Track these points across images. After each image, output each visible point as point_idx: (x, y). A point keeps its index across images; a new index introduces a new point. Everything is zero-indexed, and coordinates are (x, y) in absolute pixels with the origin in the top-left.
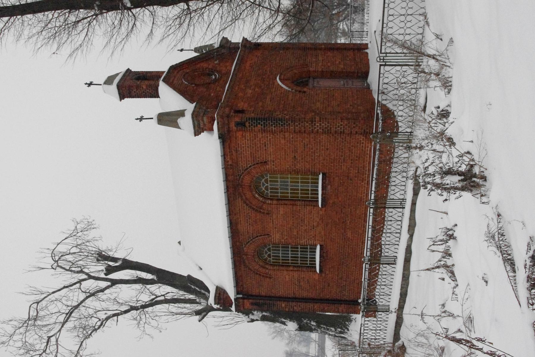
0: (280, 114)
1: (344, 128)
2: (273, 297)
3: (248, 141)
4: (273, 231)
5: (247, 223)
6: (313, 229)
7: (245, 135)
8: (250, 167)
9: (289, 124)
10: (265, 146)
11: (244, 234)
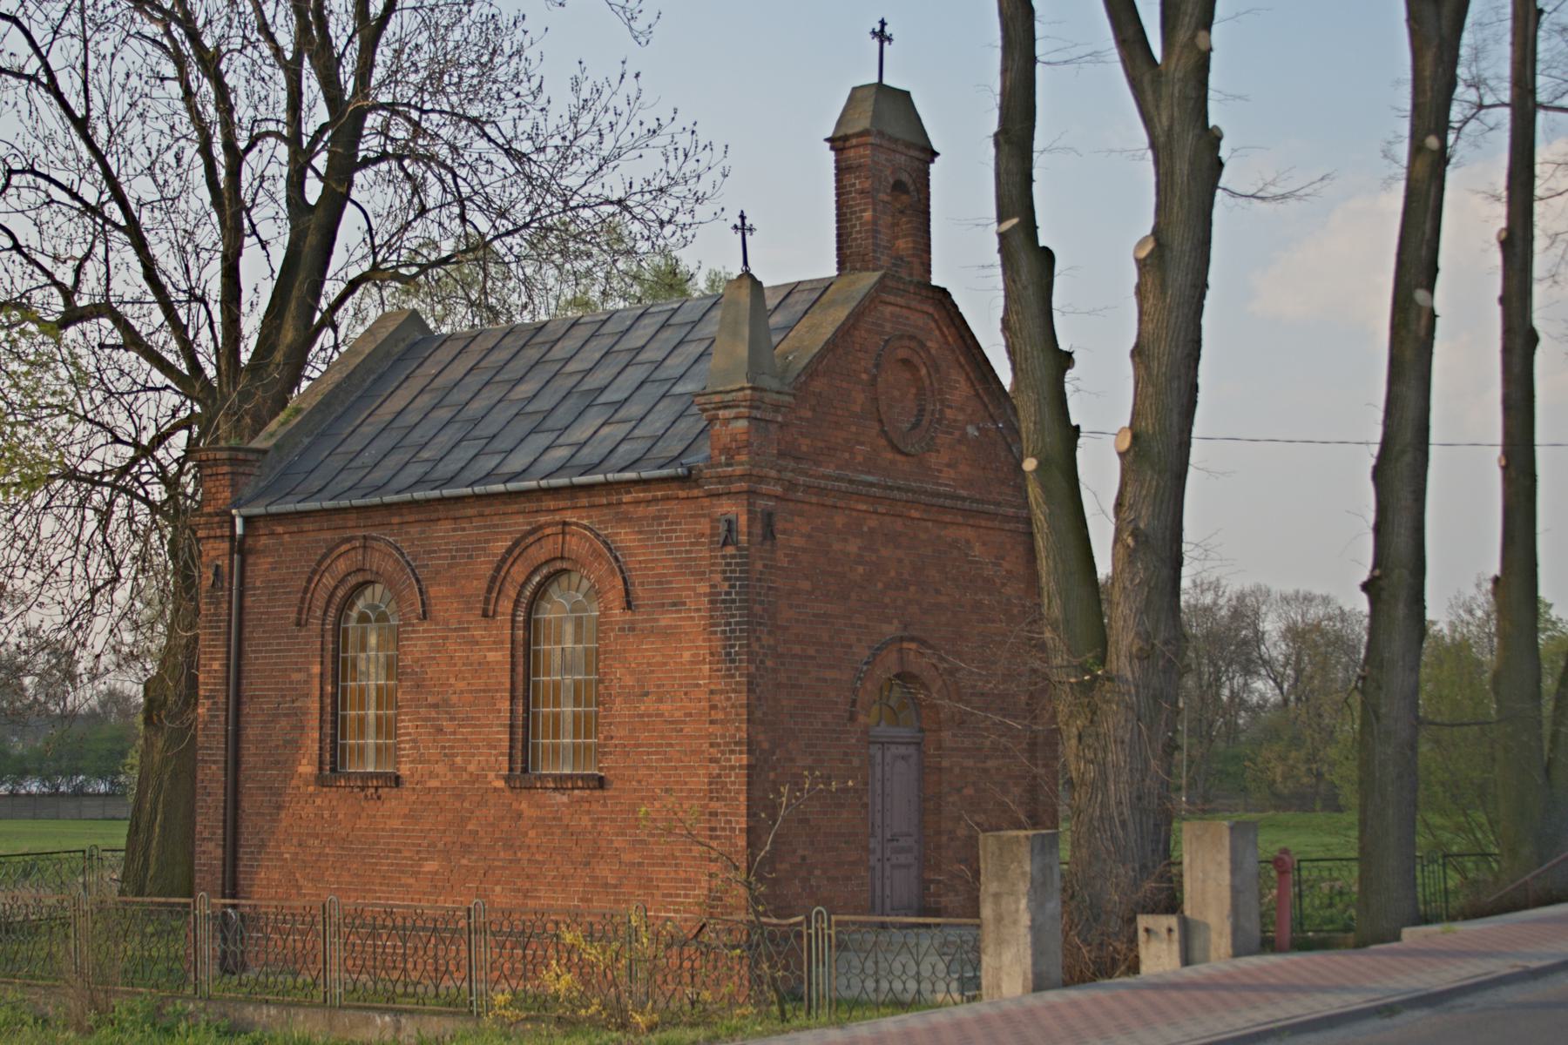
0: (762, 647)
1: (726, 837)
2: (1172, 179)
3: (687, 552)
4: (435, 631)
5: (457, 551)
6: (446, 755)
7: (703, 544)
8: (616, 559)
9: (733, 676)
10: (674, 604)
11: (426, 539)
